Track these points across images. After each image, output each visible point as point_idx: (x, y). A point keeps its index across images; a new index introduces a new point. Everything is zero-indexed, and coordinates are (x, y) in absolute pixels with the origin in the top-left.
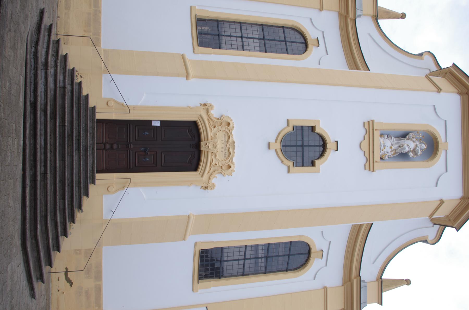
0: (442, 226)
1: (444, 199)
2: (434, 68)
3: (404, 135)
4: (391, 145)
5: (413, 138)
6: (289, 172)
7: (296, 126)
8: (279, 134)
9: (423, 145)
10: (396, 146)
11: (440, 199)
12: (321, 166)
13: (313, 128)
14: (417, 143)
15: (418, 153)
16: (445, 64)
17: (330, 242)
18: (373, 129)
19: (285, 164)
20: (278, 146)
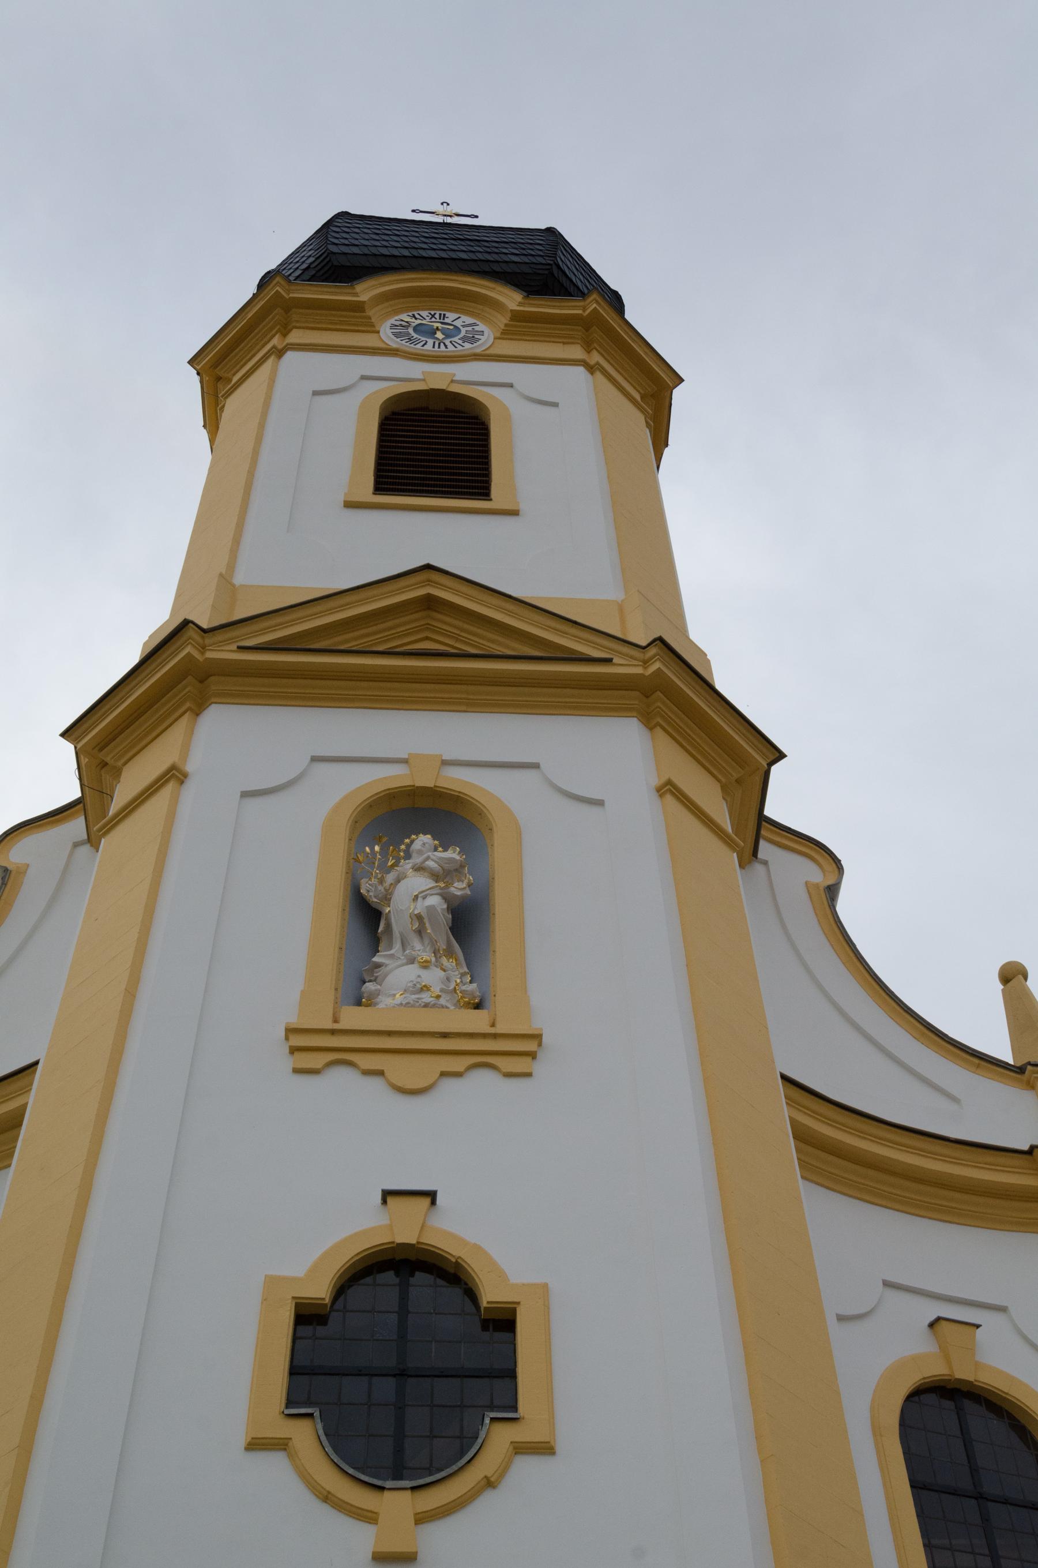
0: (763, 832)
1: (655, 781)
2: (76, 827)
3: (369, 917)
4: (416, 965)
5: (381, 881)
6: (545, 1449)
7: (289, 1403)
8: (327, 1498)
9: (417, 845)
10: (417, 945)
11: (655, 796)
12: (515, 1278)
13: (307, 1317)
14: (407, 866)
15: (451, 860)
16: (55, 778)
17: (886, 1284)
18: (333, 1032)
19: (504, 1470)
20: (397, 1504)
